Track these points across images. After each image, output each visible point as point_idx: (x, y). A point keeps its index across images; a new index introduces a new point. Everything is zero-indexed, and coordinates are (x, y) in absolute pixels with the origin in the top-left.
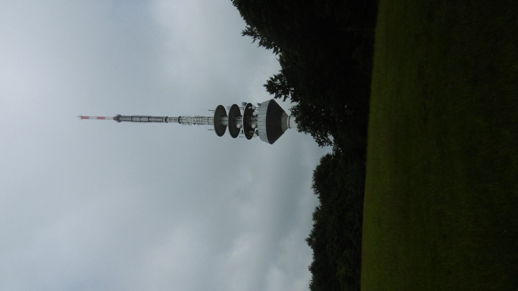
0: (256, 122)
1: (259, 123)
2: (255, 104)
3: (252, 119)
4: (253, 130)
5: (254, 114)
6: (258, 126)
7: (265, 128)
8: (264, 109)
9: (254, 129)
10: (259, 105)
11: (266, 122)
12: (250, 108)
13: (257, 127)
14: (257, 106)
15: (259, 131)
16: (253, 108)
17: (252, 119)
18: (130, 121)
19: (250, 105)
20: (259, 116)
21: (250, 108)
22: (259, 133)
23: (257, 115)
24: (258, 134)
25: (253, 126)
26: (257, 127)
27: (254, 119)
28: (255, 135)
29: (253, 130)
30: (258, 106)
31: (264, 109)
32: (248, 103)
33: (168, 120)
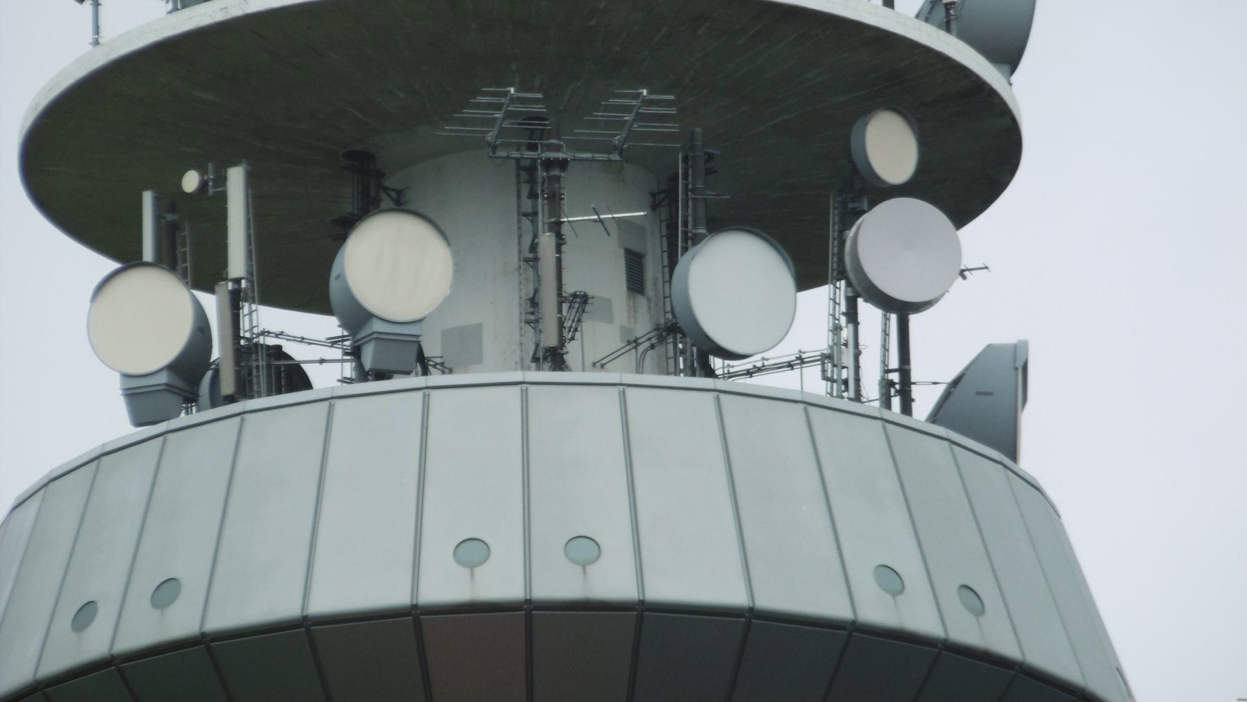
0: (498, 316)
1: (475, 415)
2: (984, 285)
3: (594, 236)
4: (299, 274)
5: (732, 278)
6: (395, 406)
7: (360, 577)
8: (880, 536)
9: (306, 284)
10: (986, 409)
11: (529, 616)
12: (890, 146)
13: (384, 354)
14: (942, 351)
15: (273, 423)
16: (889, 239)
17: (594, 236)
18: (884, 362)
19: (973, 157)
20: (673, 410)
21: (890, 146)
22: (204, 438)
23: (688, 347)
24: (183, 386)
25: (394, 262)
26: (384, 354)
27: (595, 269)
28: (163, 313)
29: (299, 274)
30: (934, 370)
31: (880, 536)
32: (1026, 91)
33: (966, 273)
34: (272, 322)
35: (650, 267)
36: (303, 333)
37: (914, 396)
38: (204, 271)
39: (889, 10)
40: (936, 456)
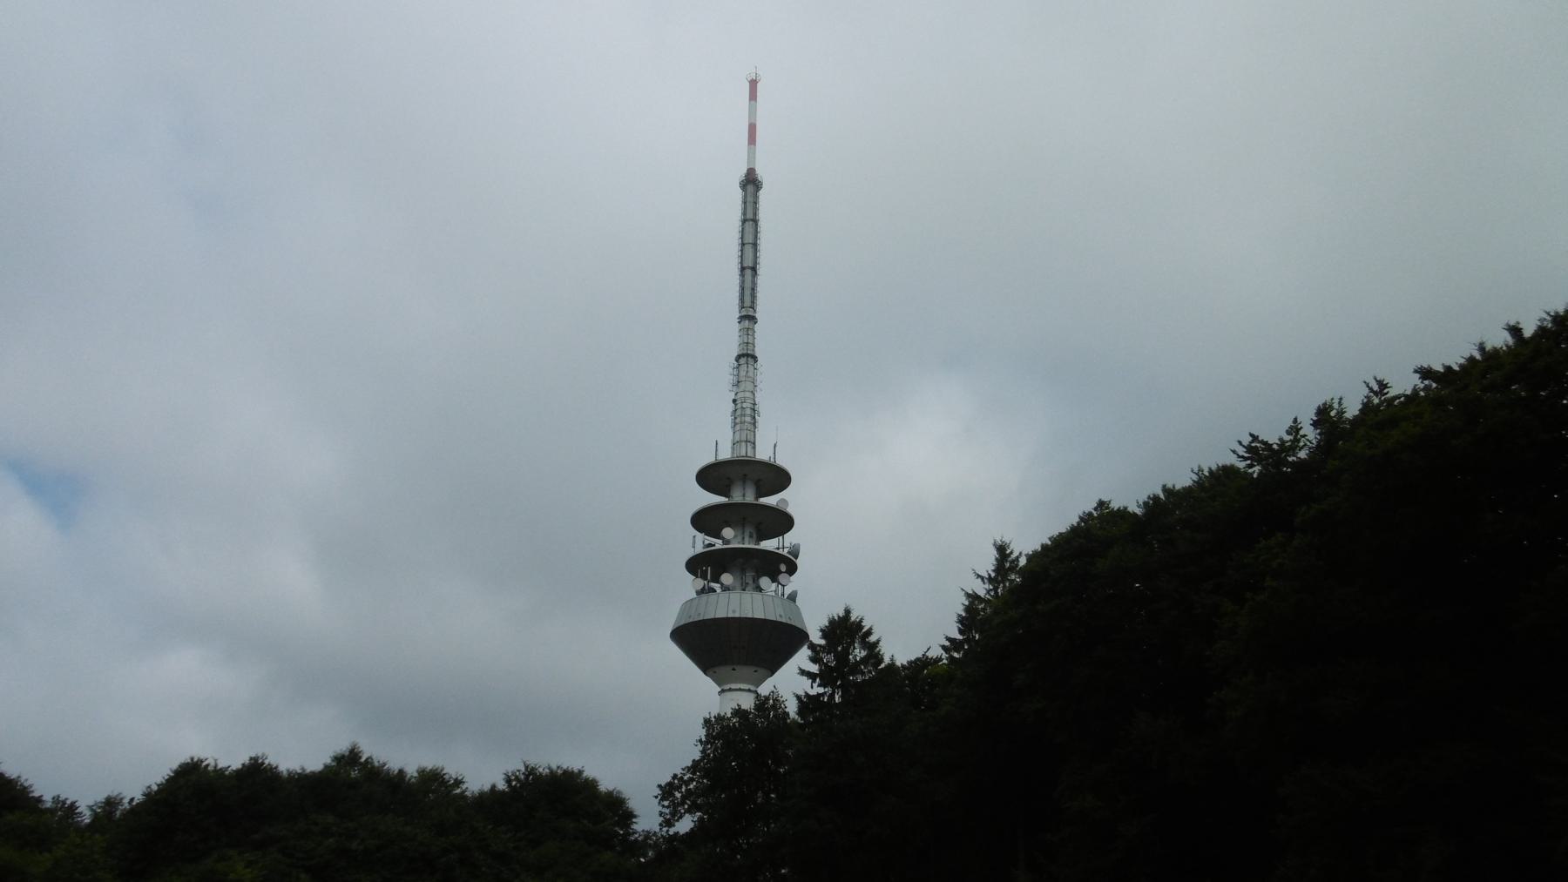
0: (738, 585)
1: (735, 596)
2: (794, 583)
4: (716, 579)
5: (765, 582)
7: (721, 614)
8: (780, 611)
10: (793, 597)
12: (783, 568)
13: (725, 588)
14: (788, 590)
15: (712, 596)
16: (782, 578)
17: (749, 575)
18: (744, 213)
19: (792, 569)
20: (757, 596)
21: (783, 568)
22: (704, 597)
24: (701, 592)
25: (727, 578)
26: (725, 588)
28: (700, 583)
29: (716, 579)
31: (780, 611)
32: (798, 562)
34: (713, 585)
35: (756, 580)
36: (716, 586)
37: (487, 787)
38: (704, 577)
39: (761, 173)
40: (788, 603)
